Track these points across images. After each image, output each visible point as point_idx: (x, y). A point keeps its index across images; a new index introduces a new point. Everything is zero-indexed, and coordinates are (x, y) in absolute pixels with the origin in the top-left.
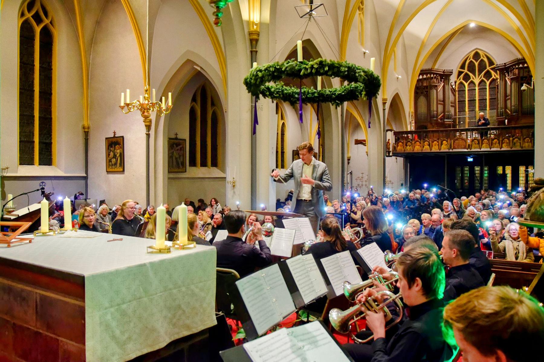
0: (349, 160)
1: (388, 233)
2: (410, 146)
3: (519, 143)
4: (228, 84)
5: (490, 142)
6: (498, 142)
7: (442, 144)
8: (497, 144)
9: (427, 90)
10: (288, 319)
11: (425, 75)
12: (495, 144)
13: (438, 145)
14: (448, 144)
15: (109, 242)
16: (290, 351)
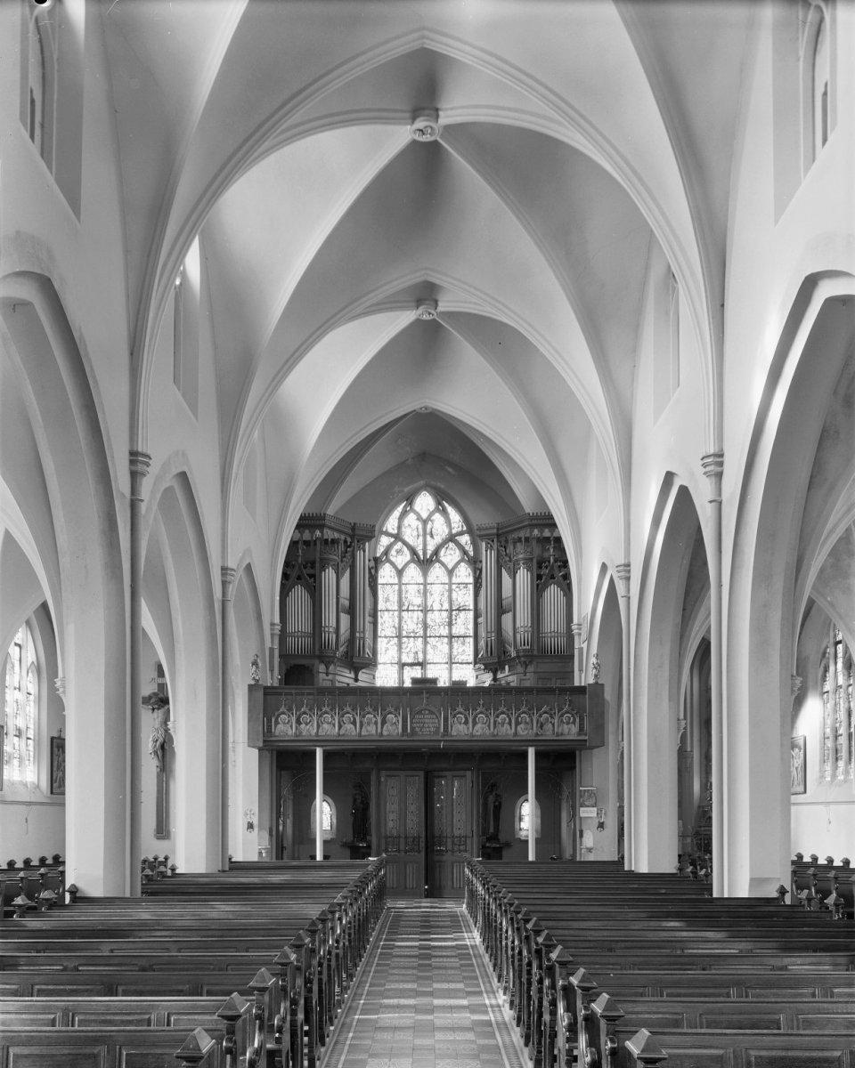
4: (228, 779)
5: (492, 721)
9: (311, 571)
10: (155, 1036)
11: (307, 531)
12: (503, 726)
16: (499, 1019)
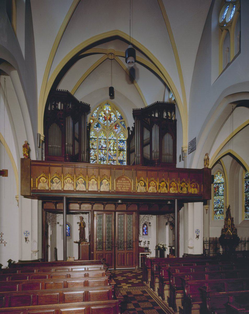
0: (198, 237)
1: (82, 202)
2: (57, 183)
3: (186, 188)
6: (165, 185)
7: (101, 184)
8: (164, 188)
13: (97, 184)
14: (109, 184)
15: (247, 169)
